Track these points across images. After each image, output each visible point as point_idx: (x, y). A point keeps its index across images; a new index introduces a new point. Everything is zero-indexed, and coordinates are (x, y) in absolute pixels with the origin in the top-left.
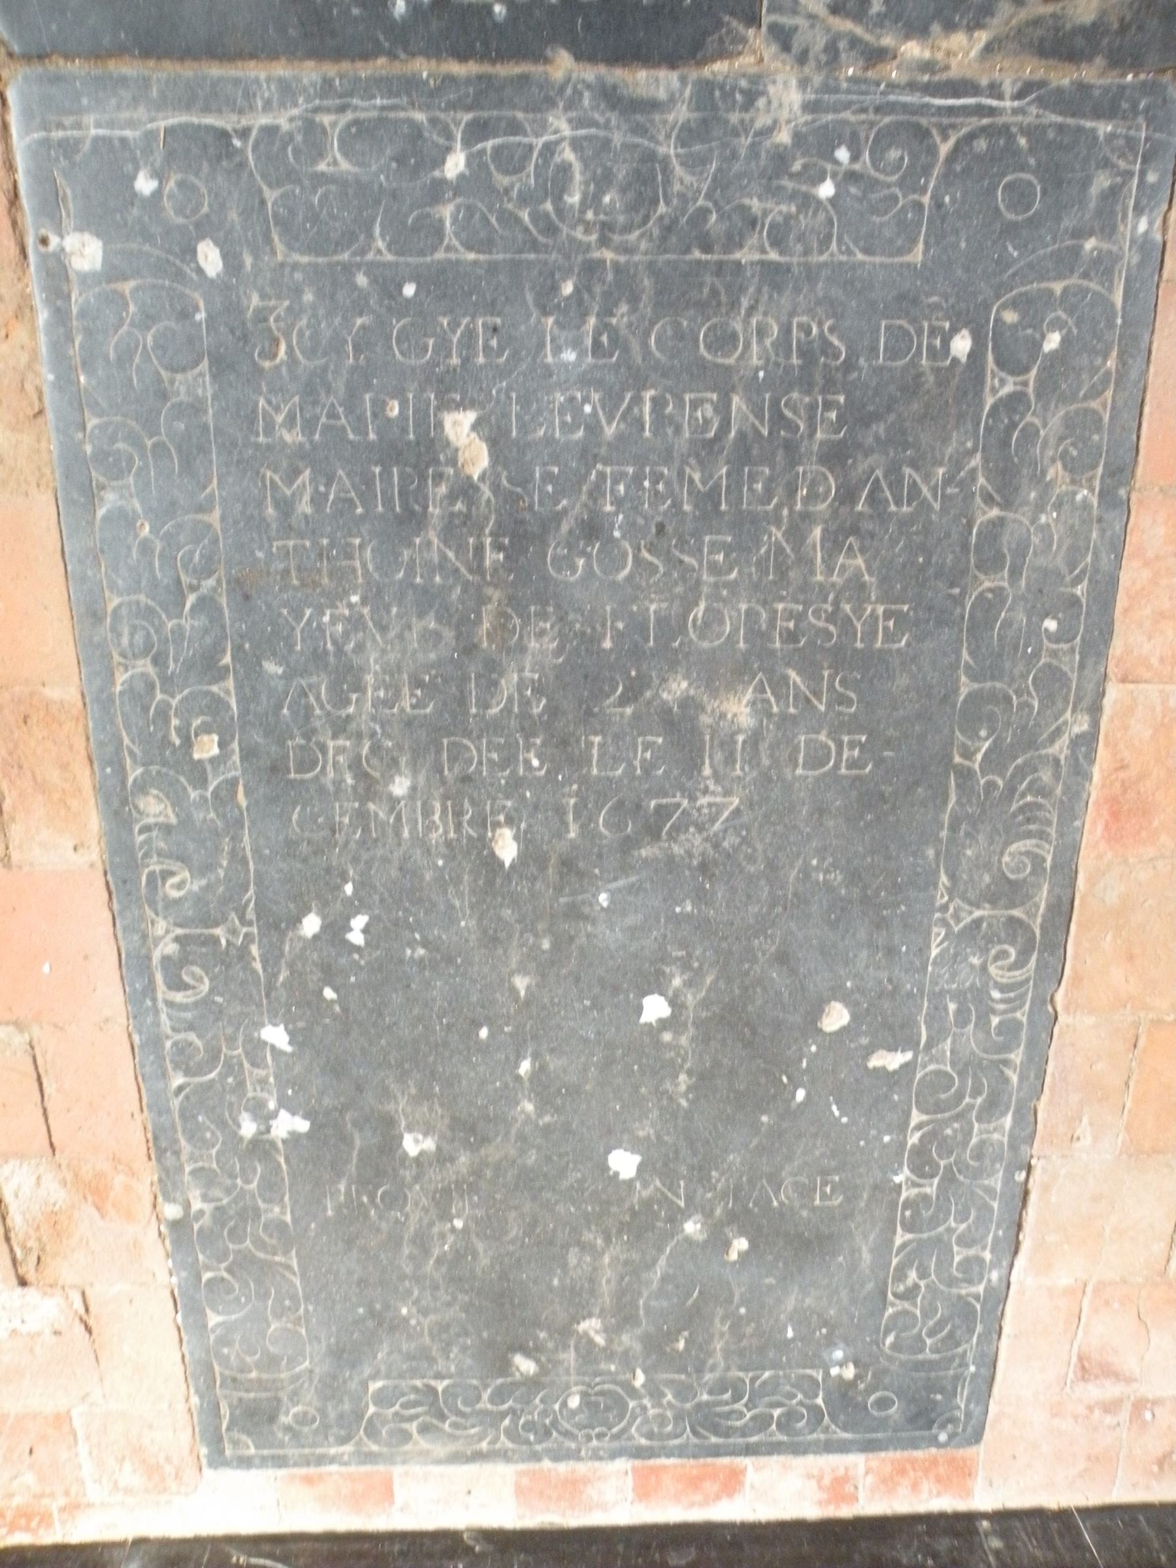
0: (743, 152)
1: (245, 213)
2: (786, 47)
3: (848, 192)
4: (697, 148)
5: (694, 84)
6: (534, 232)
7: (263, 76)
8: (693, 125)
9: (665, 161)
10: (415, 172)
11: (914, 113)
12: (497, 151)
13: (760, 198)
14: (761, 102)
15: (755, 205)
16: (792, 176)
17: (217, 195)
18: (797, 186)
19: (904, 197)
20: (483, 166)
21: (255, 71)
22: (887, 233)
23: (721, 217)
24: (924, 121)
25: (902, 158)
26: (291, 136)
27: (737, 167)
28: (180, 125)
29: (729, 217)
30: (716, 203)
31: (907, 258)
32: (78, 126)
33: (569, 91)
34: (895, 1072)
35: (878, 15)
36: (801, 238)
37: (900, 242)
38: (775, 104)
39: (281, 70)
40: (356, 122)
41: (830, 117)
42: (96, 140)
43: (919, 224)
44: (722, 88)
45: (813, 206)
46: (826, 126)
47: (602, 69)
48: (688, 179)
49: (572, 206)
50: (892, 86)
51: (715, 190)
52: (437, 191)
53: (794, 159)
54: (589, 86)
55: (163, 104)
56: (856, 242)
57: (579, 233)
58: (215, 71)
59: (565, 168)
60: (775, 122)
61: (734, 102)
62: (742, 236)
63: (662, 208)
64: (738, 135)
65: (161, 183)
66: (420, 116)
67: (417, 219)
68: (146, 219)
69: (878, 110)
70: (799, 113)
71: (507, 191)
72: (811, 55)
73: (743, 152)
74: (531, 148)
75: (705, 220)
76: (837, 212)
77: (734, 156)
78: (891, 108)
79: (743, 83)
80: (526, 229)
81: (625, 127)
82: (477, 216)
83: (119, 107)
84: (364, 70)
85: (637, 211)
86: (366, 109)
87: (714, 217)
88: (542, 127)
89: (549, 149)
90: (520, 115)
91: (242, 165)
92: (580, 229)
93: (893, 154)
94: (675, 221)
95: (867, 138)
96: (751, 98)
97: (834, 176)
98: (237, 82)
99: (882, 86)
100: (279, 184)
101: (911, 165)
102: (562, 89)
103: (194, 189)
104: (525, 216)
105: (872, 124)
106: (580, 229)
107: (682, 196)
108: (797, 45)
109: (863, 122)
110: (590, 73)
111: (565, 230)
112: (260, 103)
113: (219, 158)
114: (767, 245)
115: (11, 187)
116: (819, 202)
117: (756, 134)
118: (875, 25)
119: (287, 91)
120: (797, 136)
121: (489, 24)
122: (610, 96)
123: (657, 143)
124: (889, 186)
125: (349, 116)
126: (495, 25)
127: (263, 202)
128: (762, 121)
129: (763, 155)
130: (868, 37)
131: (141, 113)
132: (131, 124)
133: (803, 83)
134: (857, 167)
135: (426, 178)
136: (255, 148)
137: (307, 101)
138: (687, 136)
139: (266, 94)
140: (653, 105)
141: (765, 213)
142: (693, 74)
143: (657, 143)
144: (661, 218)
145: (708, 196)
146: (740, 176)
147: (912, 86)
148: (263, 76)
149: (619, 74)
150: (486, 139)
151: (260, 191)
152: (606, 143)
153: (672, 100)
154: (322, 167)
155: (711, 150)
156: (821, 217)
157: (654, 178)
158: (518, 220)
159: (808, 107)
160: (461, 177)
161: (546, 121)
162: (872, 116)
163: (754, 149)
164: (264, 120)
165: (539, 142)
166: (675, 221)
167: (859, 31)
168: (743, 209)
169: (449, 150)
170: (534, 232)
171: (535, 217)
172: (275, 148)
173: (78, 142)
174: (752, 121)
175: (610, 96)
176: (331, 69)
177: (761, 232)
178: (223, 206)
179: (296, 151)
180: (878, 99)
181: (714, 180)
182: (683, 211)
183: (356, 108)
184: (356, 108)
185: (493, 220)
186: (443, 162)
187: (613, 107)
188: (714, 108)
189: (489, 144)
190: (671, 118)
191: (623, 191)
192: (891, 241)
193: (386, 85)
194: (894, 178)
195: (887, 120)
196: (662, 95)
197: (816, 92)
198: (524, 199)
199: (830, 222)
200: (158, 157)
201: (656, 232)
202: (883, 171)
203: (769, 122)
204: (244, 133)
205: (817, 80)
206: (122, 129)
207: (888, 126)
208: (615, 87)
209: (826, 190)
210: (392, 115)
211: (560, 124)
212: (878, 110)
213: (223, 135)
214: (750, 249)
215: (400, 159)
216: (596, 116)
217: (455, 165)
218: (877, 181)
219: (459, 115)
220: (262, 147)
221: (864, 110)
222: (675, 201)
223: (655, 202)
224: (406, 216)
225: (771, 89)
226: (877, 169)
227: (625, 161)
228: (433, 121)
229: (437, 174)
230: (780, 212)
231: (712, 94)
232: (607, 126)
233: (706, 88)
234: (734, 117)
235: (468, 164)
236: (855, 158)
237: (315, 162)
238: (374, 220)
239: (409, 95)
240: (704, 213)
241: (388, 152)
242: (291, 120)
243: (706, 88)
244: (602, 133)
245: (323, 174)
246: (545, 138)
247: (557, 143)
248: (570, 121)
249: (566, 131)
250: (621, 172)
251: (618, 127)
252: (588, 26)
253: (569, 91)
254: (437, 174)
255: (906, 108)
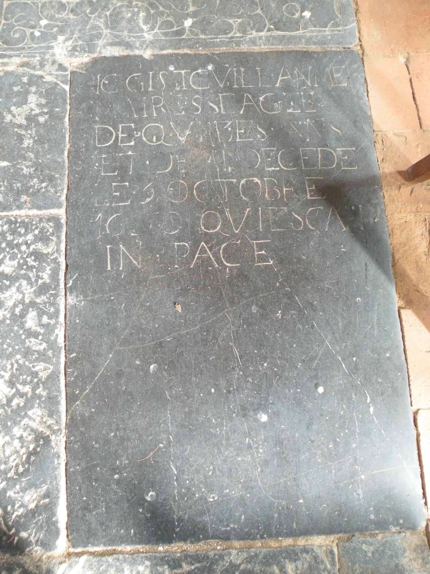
0: (77, 32)
1: (269, 6)
2: (60, 65)
3: (35, 22)
4: (95, 32)
5: (96, 51)
6: (157, 3)
7: (263, 47)
8: (96, 39)
9: (107, 27)
10: (204, 19)
11: (9, 48)
12: (172, 27)
13: (70, 18)
14: (70, 48)
15: (71, 16)
16: (57, 26)
17: (280, 11)
18: (55, 23)
19: (12, 22)
20: (177, 22)
21: (265, 48)
22: (19, 10)
23: (85, 11)
24: (5, 46)
25: (14, 34)
26: (252, 29)
27: (79, 27)
28: (294, 31)
29: (81, 12)
30: (87, 16)
31: (9, 2)
32: (332, 31)
33: (144, 46)
34: (27, 96)
35: (24, 77)
36: (53, 7)
37: (13, 7)
38: (64, 49)
39: (256, 49)
40: (227, 34)
41: (43, 45)
42: (326, 27)
43: (6, 13)
44: (85, 51)
45: (49, 17)
46: (44, 42)
47: (131, 53)
48: (98, 23)
49: (143, 12)
50: (19, 56)
51: (87, 20)
52: (194, 15)
53: (56, 31)
54: (137, 48)
55: (300, 38)
56: (31, 6)
57: (140, 4)
58: (280, 48)
59: (145, 23)
60: (64, 43)
61: (80, 48)
62: (77, 6)
63: (108, 13)
64: (79, 37)
65: (301, 15)
66: (202, 36)
67: (203, 6)
68: (306, 4)
69: (24, 48)
70: (55, 46)
71: (168, 16)
72: (50, 63)
73: (77, 32)
74: (159, 29)
75: (91, 11)
76: (39, 16)
77: (80, 31)
78: (18, 49)
79: (77, 53)
80: (160, 4)
81: (123, 37)
82: (179, 7)
83: (317, 36)
84: (224, 49)
85: (118, 12)
86: (223, 38)
87: (88, 11)
88: (154, 35)
89: (152, 28)
90: (163, 38)
91: (270, 20)
92: (140, 5)
93: (17, 36)
94: (103, 10)
95: (28, 40)
96: (74, 49)
97: (41, 27)
98: (272, 44)
99: (22, 55)
100: (256, 15)
101: (10, 32)
102: (147, 47)
103: (288, 13)
104: (161, 9)
105: (26, 44)
106: (140, 5)
107: (100, 17)
108: (56, 66)
109: (29, 45)
110: (137, 52)
111: (146, 5)
112: (264, 38)
113: (279, 22)
114: (67, 5)
115: (358, 14)
116: (46, 18)
117: (71, 38)
118: (25, 73)
119: (253, 42)
120: (55, 38)
121: (176, 64)
122: (128, 46)
123: (110, 33)
124: (19, 25)
125: (229, 36)
126: (173, 64)
127: (262, 9)
128: (70, 43)
129: (69, 32)
130: (28, 70)
131: (308, 35)
132: (312, 31)
133: (53, 55)
134: (32, 30)
135: (199, 18)
136: (266, 25)
137: (245, 40)
138: (99, 36)
139: (261, 41)
140: (112, 44)
141: (67, 14)
142: (95, 55)
143: (110, 33)
144: (108, 10)
145: (90, 18)
146: (78, 25)
147: (10, 57)
148: (263, 47)
149: (126, 53)
150: (176, 30)
151: (263, 12)
152: (130, 31)
153: (104, 47)
154: (240, 20)
155: (89, 32)
156: (45, 14)
157: (111, 22)
158: (164, 7)
159: (52, 47)
160: (186, 19)
161: (154, 37)
162: (26, 46)
163: (72, 33)
164: (262, 34)
165: (156, 30)
166: (103, 10)
167: (32, 72)
168: (76, 14)
169: (191, 27)
170: (157, 3)
171: (157, 8)
172: (257, 25)
173: (332, 26)
174: (73, 43)
175: (128, 46)
176: (236, 49)
177: (69, 8)
178: (277, 8)
179: (249, 24)
180: (23, 51)
181: (88, 23)
182: (100, 13)
183: (227, 38)
184: (227, 38)
185: (173, 6)
186: (193, 23)
187: (127, 42)
188: (88, 45)
189: (175, 29)
190: (105, 41)
191: (123, 18)
192: (17, 7)
193: (215, 45)
194: (17, 28)
195: (20, 46)
196: (109, 48)
197: (48, 52)
198: (162, 14)
199: (41, 12)
200: (302, 22)
201: (110, 6)
202: (20, 30)
203: (66, 42)
204: (269, 30)
205: (47, 56)
206: (316, 30)
207: (20, 44)
208: (127, 49)
209: (43, 22)
210: (213, 36)
211: (148, 37)
212: (24, 48)
213: (277, 29)
214: (73, 3)
215: (209, 23)
216: (134, 40)
217: (188, 23)
218: (23, 27)
219: (187, 37)
220: (263, 26)
221: (29, 48)
222: (103, 16)
223: (110, 15)
224: (207, 6)
225: (66, 53)
226: (23, 30)
227: (123, 26)
228: (197, 35)
229: (195, 20)
230: (61, 15)
231: (89, 48)
232: (130, 37)
233: (91, 49)
234: (80, 42)
235: (183, 23)
236: (32, 33)
237: (242, 22)
238: (219, 4)
239: (206, 42)
240: (92, 13)
241: (214, 25)
242: (251, 34)
243: (91, 49)
244: (132, 34)
245: (239, 18)
246: (154, 32)
247: (149, 31)
248: (144, 37)
249: (145, 35)
250: (124, 23)
251: (125, 37)
252: (137, 65)
253: (144, 46)
254: (195, 20)
255: (13, 50)
